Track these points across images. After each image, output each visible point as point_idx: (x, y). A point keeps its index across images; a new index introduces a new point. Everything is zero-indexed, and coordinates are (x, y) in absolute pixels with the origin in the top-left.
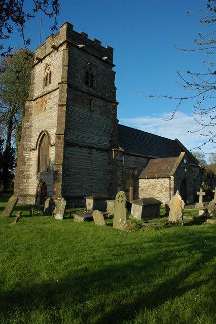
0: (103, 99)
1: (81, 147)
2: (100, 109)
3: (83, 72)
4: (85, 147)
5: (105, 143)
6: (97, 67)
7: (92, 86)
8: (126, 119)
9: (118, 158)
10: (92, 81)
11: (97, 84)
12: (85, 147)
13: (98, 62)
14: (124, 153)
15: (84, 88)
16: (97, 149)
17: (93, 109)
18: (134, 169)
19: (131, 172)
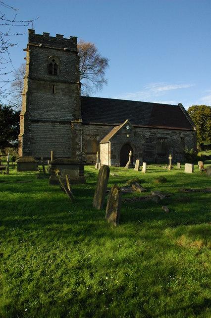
0: (64, 82)
1: (44, 122)
2: (62, 91)
3: (46, 65)
4: (48, 122)
5: (67, 116)
6: (59, 58)
7: (56, 74)
8: (84, 92)
9: (77, 128)
10: (56, 70)
11: (60, 71)
12: (48, 122)
13: (60, 53)
14: (83, 124)
15: (47, 77)
16: (60, 122)
17: (55, 92)
18: (96, 136)
19: (92, 139)
